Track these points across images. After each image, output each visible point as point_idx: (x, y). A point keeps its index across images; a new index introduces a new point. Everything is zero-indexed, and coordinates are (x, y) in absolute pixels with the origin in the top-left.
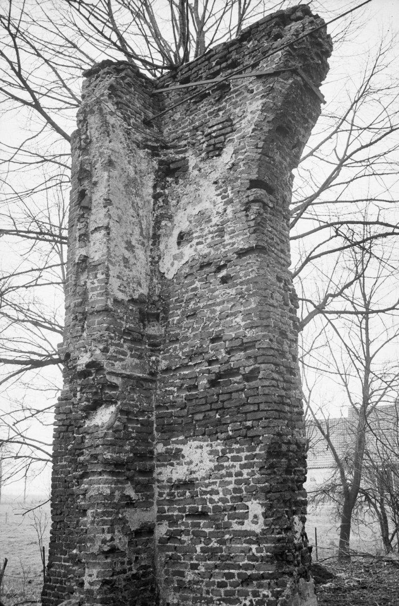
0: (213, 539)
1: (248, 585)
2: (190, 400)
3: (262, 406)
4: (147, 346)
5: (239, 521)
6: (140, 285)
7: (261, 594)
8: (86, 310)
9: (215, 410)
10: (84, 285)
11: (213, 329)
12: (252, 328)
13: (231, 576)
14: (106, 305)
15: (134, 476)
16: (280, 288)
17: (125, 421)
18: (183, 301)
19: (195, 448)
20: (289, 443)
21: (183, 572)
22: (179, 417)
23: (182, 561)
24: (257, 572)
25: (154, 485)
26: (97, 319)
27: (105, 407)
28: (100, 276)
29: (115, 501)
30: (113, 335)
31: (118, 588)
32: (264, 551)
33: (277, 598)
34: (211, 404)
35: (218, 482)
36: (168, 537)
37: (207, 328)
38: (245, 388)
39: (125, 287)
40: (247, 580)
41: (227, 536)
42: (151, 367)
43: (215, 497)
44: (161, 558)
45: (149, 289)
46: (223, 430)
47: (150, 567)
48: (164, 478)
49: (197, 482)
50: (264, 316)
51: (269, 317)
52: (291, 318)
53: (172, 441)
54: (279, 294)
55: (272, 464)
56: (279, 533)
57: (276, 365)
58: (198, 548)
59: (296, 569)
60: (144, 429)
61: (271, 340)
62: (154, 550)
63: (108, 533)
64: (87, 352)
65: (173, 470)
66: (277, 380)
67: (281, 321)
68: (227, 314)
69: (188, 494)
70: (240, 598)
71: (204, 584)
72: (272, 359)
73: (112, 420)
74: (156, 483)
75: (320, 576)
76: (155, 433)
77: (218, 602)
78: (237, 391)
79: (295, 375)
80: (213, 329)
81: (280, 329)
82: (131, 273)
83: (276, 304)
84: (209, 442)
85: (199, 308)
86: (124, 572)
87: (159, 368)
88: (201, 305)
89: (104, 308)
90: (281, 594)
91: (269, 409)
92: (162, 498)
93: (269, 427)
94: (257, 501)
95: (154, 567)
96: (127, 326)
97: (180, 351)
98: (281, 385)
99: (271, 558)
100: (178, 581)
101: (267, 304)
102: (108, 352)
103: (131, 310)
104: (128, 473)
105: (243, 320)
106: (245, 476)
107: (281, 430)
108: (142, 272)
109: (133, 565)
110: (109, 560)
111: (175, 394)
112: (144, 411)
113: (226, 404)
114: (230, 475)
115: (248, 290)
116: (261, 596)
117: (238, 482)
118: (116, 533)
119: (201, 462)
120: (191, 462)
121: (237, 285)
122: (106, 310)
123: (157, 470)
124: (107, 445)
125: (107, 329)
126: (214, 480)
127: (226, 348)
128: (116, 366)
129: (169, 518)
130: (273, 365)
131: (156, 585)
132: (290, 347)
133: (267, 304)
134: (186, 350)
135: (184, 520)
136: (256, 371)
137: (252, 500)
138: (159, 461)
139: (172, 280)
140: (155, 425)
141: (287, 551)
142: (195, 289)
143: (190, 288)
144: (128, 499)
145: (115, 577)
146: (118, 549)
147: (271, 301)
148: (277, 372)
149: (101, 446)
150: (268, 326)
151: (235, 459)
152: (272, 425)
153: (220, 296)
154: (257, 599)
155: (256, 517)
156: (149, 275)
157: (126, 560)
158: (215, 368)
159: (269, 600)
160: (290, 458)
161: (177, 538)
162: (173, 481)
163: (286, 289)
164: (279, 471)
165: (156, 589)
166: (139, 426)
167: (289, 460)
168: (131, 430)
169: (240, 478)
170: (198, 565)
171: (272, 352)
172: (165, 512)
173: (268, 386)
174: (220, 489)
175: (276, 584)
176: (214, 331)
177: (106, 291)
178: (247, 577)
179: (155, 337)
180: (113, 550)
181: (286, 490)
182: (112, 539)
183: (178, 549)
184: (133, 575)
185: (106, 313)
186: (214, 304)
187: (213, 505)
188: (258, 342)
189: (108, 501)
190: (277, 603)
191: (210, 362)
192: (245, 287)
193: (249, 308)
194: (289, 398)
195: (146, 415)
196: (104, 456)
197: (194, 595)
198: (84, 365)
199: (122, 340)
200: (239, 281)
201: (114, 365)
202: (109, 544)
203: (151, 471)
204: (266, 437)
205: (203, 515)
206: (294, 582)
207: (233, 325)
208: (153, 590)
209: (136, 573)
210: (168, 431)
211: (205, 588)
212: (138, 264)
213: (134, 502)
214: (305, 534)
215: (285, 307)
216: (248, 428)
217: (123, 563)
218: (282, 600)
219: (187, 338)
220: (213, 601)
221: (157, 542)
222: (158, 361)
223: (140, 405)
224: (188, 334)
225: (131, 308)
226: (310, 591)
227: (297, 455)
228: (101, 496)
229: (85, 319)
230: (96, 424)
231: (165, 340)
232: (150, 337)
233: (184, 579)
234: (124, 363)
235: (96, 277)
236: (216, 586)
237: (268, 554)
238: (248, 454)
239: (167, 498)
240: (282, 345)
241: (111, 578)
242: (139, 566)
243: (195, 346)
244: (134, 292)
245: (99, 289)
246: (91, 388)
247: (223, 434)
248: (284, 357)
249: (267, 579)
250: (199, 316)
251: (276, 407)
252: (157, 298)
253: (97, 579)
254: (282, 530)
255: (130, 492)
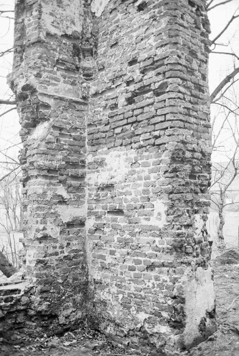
0: (126, 232)
1: (152, 270)
2: (112, 117)
3: (168, 117)
4: (82, 76)
5: (146, 217)
6: (74, 24)
7: (161, 279)
8: (24, 44)
9: (130, 123)
10: (22, 23)
11: (130, 53)
12: (162, 46)
13: (138, 262)
14: (39, 37)
15: (66, 180)
16: (192, 11)
17: (58, 135)
18: (108, 33)
19: (115, 157)
20: (193, 151)
21: (105, 256)
22: (104, 132)
23: (105, 248)
24: (158, 261)
25: (85, 188)
26: (33, 50)
27: (41, 123)
28: (35, 13)
29: (47, 199)
30: (45, 63)
31: (50, 266)
32: (165, 244)
33: (174, 283)
34: (127, 119)
35: (131, 185)
36: (95, 228)
37: (126, 53)
38: (154, 102)
39: (58, 24)
40: (151, 267)
41: (137, 230)
42: (83, 92)
43: (129, 198)
44: (89, 246)
45: (83, 28)
46: (136, 140)
47: (81, 251)
48: (92, 182)
49: (116, 185)
50: (173, 34)
51: (177, 35)
52: (202, 41)
53: (99, 153)
54: (190, 17)
55: (175, 168)
56: (178, 229)
57: (183, 79)
58: (116, 238)
59: (195, 259)
60: (76, 143)
61: (179, 57)
62: (85, 238)
63: (41, 223)
64: (23, 77)
65: (99, 176)
66: (184, 94)
67: (191, 41)
68: (141, 38)
69: (109, 195)
70: (145, 280)
71: (119, 266)
72: (179, 74)
73: (45, 134)
74: (87, 186)
75: (235, 258)
76: (87, 146)
77: (129, 282)
78: (148, 105)
79: (203, 92)
80: (130, 53)
81: (189, 48)
82: (64, 12)
83: (185, 24)
84: (125, 151)
85: (120, 37)
86: (56, 254)
87: (90, 93)
88: (121, 34)
89: (37, 40)
90: (177, 281)
91: (175, 119)
92: (91, 198)
93: (173, 135)
94: (162, 201)
95: (85, 252)
96: (61, 57)
97: (105, 76)
98: (188, 98)
99: (170, 250)
100: (101, 262)
101: (176, 23)
102: (41, 77)
103: (64, 43)
104: (60, 178)
105: (155, 41)
106: (152, 179)
107: (186, 139)
108: (76, 13)
109: (64, 249)
110: (42, 245)
111: (102, 114)
112: (76, 128)
113: (139, 118)
114: (140, 179)
115: (159, 12)
116: (161, 280)
117: (146, 185)
118: (48, 224)
119: (119, 168)
120: (111, 169)
121: (151, 9)
122: (39, 42)
123: (88, 176)
124: (40, 154)
125: (40, 58)
126: (128, 184)
127: (140, 68)
128: (49, 89)
129: (95, 214)
130: (179, 79)
131: (86, 263)
132: (200, 66)
133: (176, 23)
134: (109, 75)
135: (106, 216)
136: (164, 86)
137: (157, 199)
138: (89, 168)
139: (100, 18)
140: (87, 140)
141: (186, 244)
142: (118, 21)
143: (113, 21)
144: (60, 198)
145: (47, 258)
146: (50, 237)
147: (181, 21)
148: (184, 87)
149: (35, 155)
150: (176, 43)
151: (145, 165)
152: (176, 133)
153: (136, 23)
154: (158, 282)
155: (159, 214)
156: (83, 16)
157: (58, 245)
158: (132, 88)
159: (167, 285)
160: (194, 164)
161: (101, 230)
162: (99, 185)
163: (199, 13)
164: (181, 174)
165: (86, 267)
166: (72, 140)
167: (193, 166)
168: (64, 143)
169: (148, 181)
170: (115, 252)
171: (179, 67)
172: (93, 209)
173: (174, 98)
174: (133, 191)
175: (174, 272)
176: (130, 55)
177: (39, 25)
178: (151, 264)
179: (89, 69)
180: (45, 237)
181: (188, 192)
182: (44, 229)
183: (101, 238)
184: (65, 257)
185: (39, 44)
186: (132, 31)
187: (127, 204)
188: (167, 59)
189: (41, 198)
190: (174, 288)
191: (128, 83)
192: (157, 10)
193: (160, 28)
194: (196, 111)
195: (79, 131)
196: (38, 163)
197: (112, 275)
198: (21, 89)
199: (55, 69)
200: (151, 6)
201: (47, 89)
202: (41, 232)
203: (82, 177)
204: (171, 145)
205: (120, 212)
206: (192, 270)
207: (146, 46)
208: (83, 268)
209: (68, 255)
210: (95, 143)
211: (119, 270)
212: (72, 5)
213: (66, 200)
214: (206, 231)
215: (196, 30)
216: (157, 137)
217: (55, 247)
218: (178, 286)
219: (110, 65)
220: (125, 281)
221: (87, 232)
222: (89, 87)
223: (72, 123)
224: (112, 61)
225: (64, 42)
226: (208, 277)
227: (201, 162)
228: (36, 194)
229: (24, 51)
230: (34, 138)
231: (96, 71)
232: (84, 69)
233: (105, 262)
234: (57, 87)
235: (32, 15)
236: (127, 269)
237: (168, 246)
238: (156, 160)
239: (95, 198)
240: (191, 63)
241: (44, 259)
242: (70, 250)
243: (116, 71)
244: (67, 29)
245: (33, 24)
246: (28, 108)
247: (136, 144)
248: (193, 74)
249: (167, 266)
250: (120, 44)
251: (181, 117)
252: (90, 36)
253: (33, 259)
254: (181, 226)
255: (62, 191)
